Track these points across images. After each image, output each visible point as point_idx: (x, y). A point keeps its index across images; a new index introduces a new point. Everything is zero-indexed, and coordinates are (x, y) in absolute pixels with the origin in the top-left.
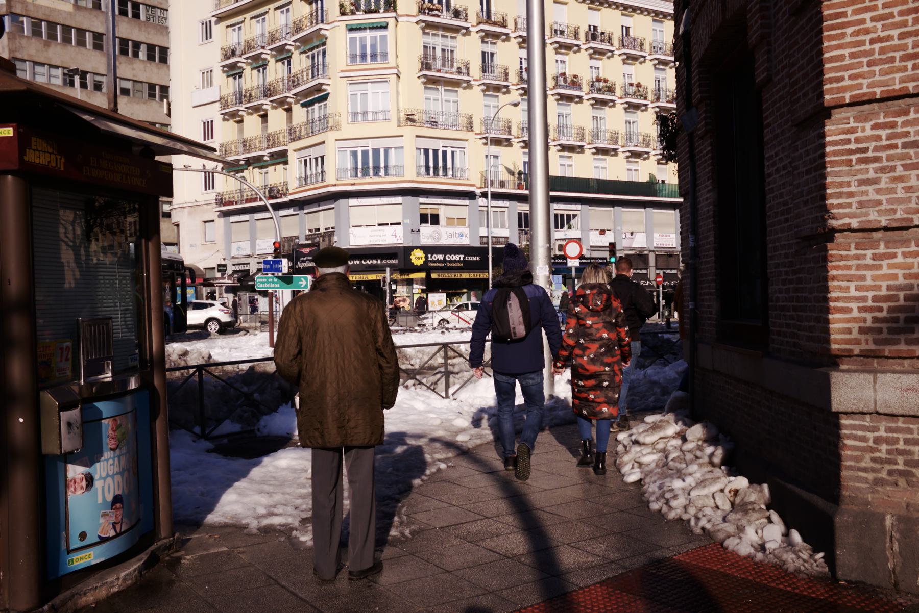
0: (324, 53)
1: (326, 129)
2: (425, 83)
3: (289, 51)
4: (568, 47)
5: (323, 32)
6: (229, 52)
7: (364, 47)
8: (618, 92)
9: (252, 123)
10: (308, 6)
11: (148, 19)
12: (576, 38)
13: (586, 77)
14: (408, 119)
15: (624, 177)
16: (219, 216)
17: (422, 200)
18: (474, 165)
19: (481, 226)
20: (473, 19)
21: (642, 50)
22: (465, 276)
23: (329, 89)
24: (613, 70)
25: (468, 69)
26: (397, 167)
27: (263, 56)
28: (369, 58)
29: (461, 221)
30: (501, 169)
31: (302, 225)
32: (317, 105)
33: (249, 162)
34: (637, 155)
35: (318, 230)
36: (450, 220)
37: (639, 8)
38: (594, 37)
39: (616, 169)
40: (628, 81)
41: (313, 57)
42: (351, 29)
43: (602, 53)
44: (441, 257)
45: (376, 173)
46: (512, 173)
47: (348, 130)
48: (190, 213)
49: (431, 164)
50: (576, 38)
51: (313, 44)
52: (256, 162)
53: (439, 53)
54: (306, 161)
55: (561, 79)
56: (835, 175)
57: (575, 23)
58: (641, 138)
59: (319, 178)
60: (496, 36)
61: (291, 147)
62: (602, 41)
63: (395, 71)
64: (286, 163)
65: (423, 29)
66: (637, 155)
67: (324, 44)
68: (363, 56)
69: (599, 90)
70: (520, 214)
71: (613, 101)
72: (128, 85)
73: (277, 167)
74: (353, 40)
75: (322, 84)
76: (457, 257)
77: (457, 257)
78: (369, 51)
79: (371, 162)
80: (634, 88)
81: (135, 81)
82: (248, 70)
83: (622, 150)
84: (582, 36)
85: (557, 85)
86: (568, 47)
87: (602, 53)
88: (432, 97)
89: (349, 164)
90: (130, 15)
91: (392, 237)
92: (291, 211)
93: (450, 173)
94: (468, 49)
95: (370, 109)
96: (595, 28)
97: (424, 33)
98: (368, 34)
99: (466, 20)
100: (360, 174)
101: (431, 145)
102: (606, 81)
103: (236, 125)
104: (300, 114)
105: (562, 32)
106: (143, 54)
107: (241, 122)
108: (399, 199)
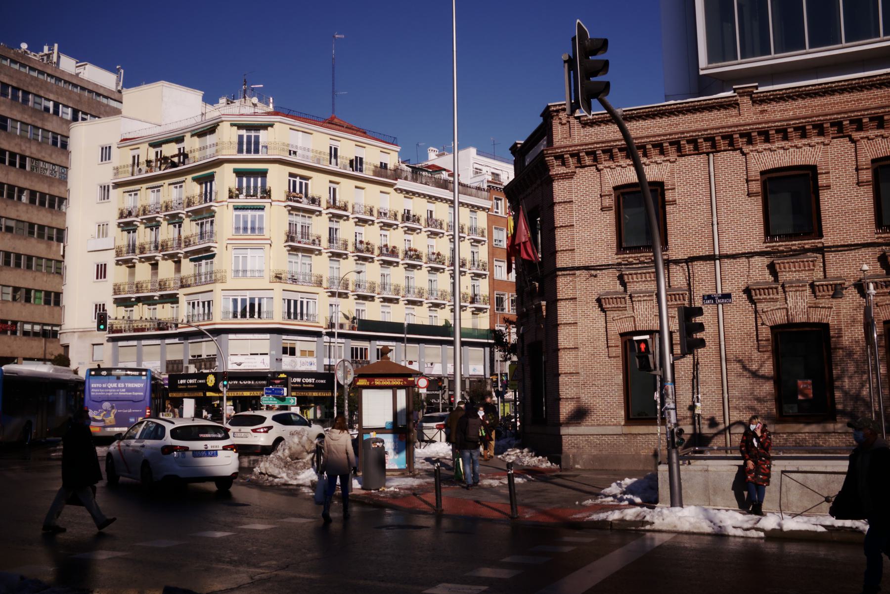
0: (212, 222)
1: (214, 282)
2: (289, 251)
3: (181, 218)
4: (390, 226)
5: (213, 208)
6: (126, 212)
7: (245, 222)
8: (424, 259)
9: (143, 271)
10: (199, 186)
11: (32, 169)
12: (396, 219)
13: (401, 248)
14: (276, 277)
15: (427, 322)
16: (108, 341)
17: (284, 337)
18: (321, 310)
19: (325, 357)
20: (324, 204)
21: (441, 228)
22: (315, 394)
23: (215, 251)
24: (421, 242)
25: (320, 241)
26: (268, 312)
27: (158, 219)
28: (249, 231)
29: (311, 353)
30: (340, 315)
31: (186, 352)
32: (204, 262)
33: (139, 300)
34: (436, 305)
35: (200, 356)
36: (303, 353)
37: (440, 198)
38: (408, 219)
39: (421, 316)
40: (431, 251)
41: (202, 224)
42: (237, 208)
43: (413, 230)
44: (299, 380)
45: (252, 316)
46: (347, 318)
47: (232, 282)
48: (80, 337)
49: (292, 310)
50: (396, 219)
51: (204, 215)
52: (148, 301)
53: (299, 229)
54: (194, 303)
55: (384, 249)
56: (561, 387)
57: (395, 209)
58: (439, 293)
59: (206, 318)
60: (340, 217)
61: (181, 292)
62: (414, 221)
63: (269, 242)
64: (177, 302)
65: (289, 211)
66: (436, 305)
67: (213, 216)
68: (245, 229)
69: (411, 257)
70: (352, 348)
71: (421, 266)
72: (12, 224)
73: (165, 305)
74: (237, 217)
75: (211, 247)
76: (310, 380)
77: (310, 380)
78: (249, 226)
79: (251, 309)
80: (435, 256)
81: (18, 221)
82: (141, 227)
83: (426, 301)
84: (399, 217)
85: (381, 254)
86: (390, 226)
87: (413, 230)
88: (293, 261)
89: (231, 309)
90: (18, 166)
91: (262, 364)
92: (176, 340)
93: (305, 318)
94: (319, 226)
95: (249, 268)
96: (409, 211)
97: (290, 214)
98: (249, 213)
99: (319, 205)
100: (239, 317)
101: (293, 296)
102: (416, 251)
103: (128, 269)
104: (188, 267)
105: (385, 214)
106: (24, 199)
107: (134, 266)
108: (268, 336)
